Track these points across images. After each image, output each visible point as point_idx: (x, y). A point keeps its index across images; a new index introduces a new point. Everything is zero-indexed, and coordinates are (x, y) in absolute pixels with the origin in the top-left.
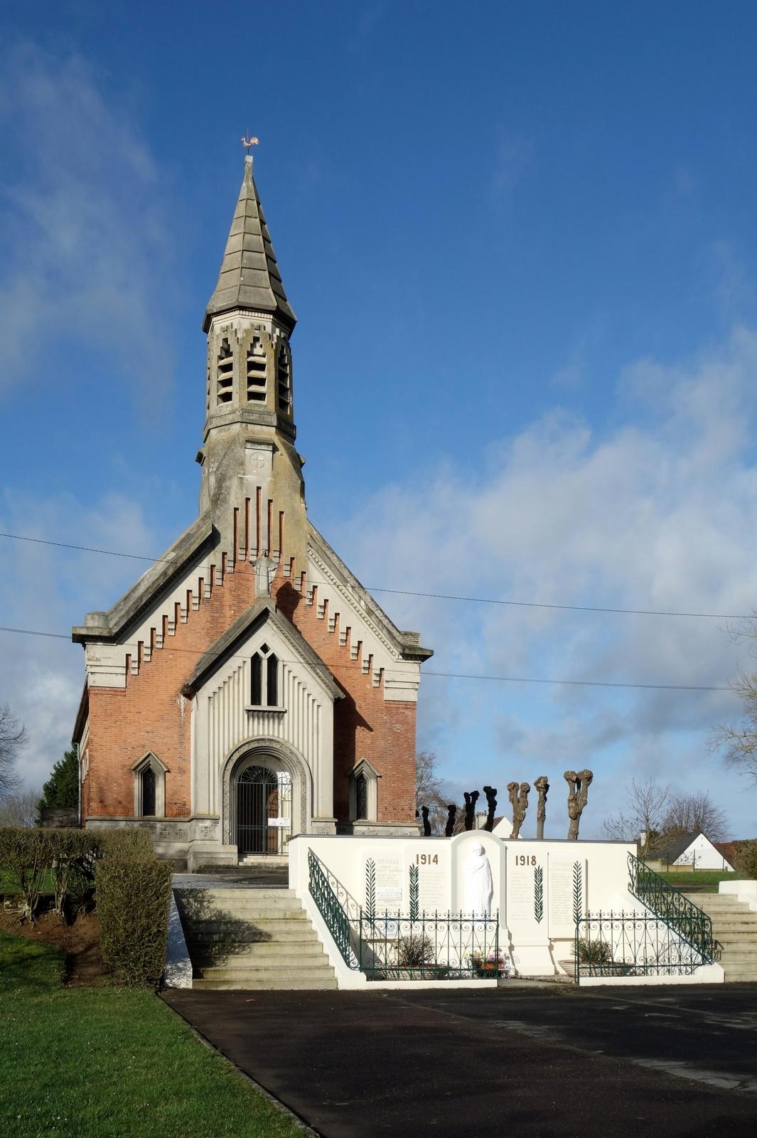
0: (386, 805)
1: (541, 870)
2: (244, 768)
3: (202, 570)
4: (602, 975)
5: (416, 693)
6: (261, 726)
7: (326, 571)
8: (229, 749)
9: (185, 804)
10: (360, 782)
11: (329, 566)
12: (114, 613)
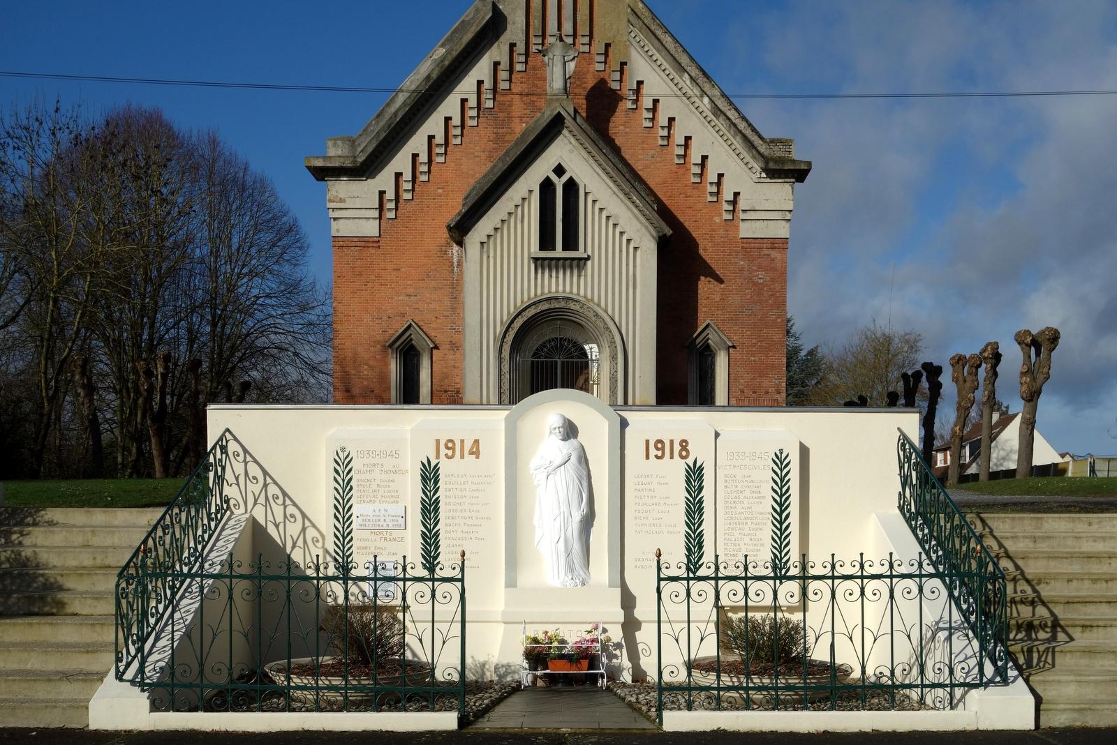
0: (741, 387)
1: (701, 468)
2: (534, 342)
3: (481, 70)
4: (689, 707)
5: (787, 225)
6: (554, 280)
7: (655, 58)
8: (509, 313)
9: (458, 392)
10: (706, 357)
11: (658, 50)
12: (363, 137)
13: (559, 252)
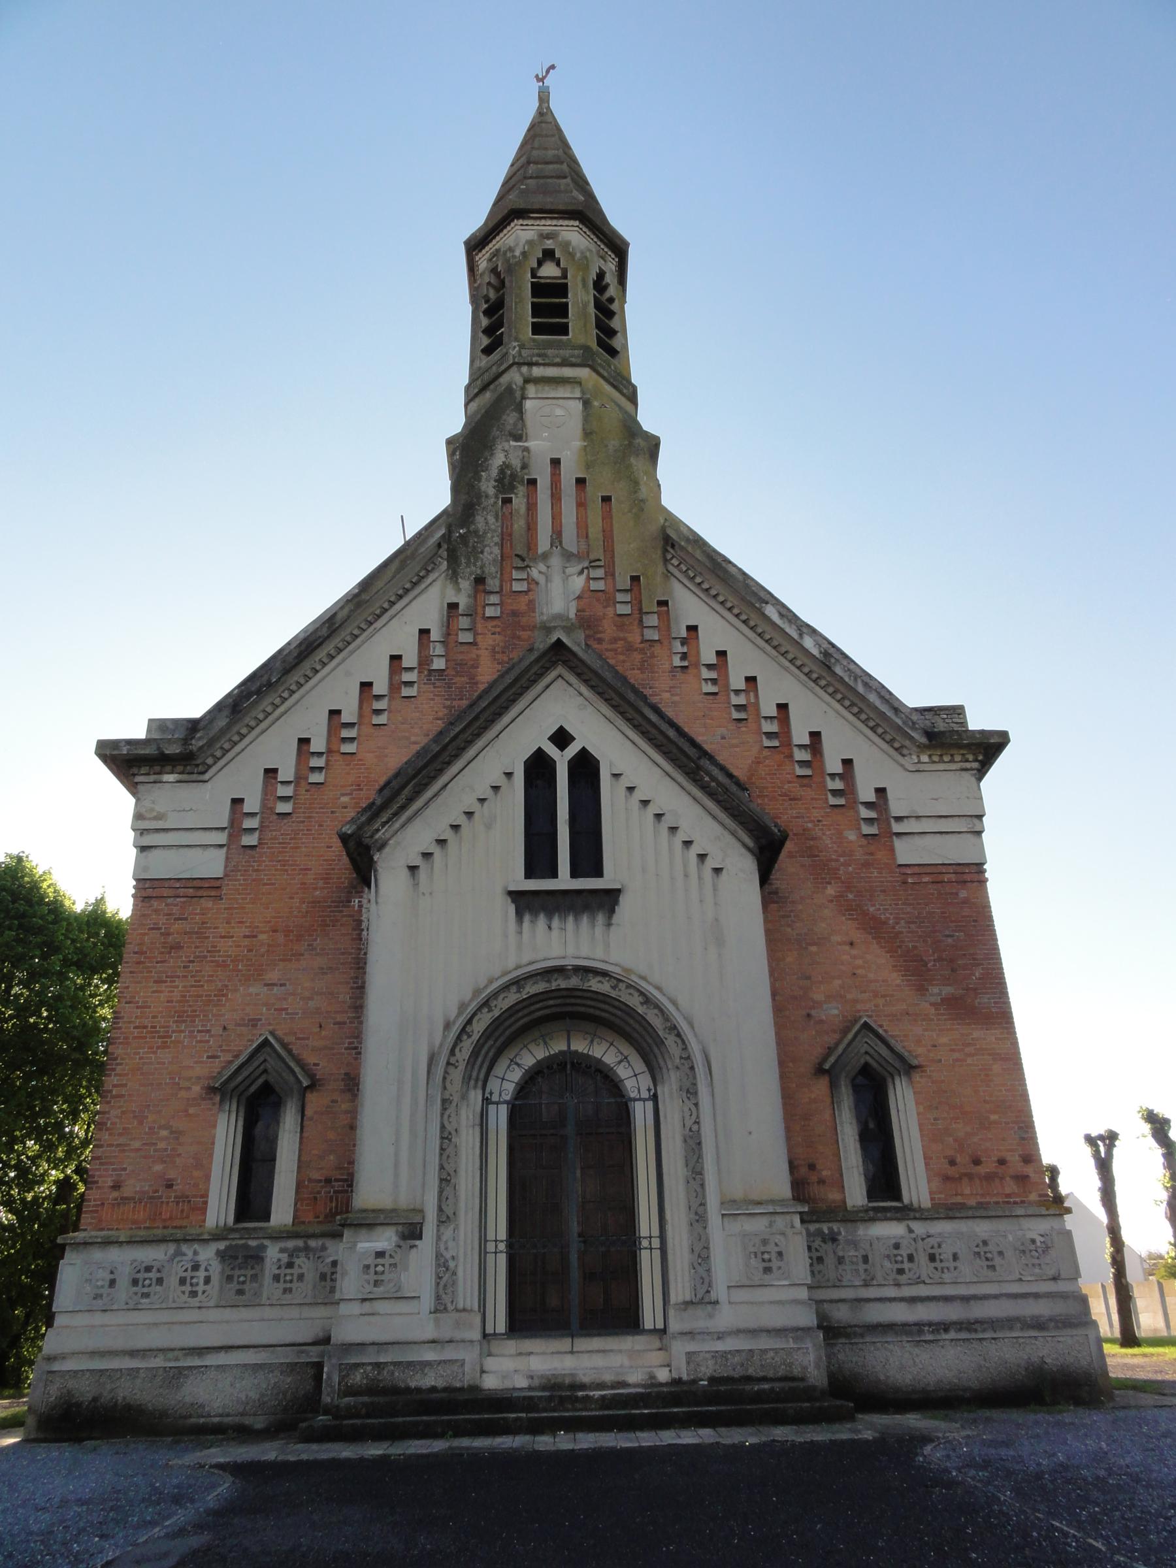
13: (564, 880)
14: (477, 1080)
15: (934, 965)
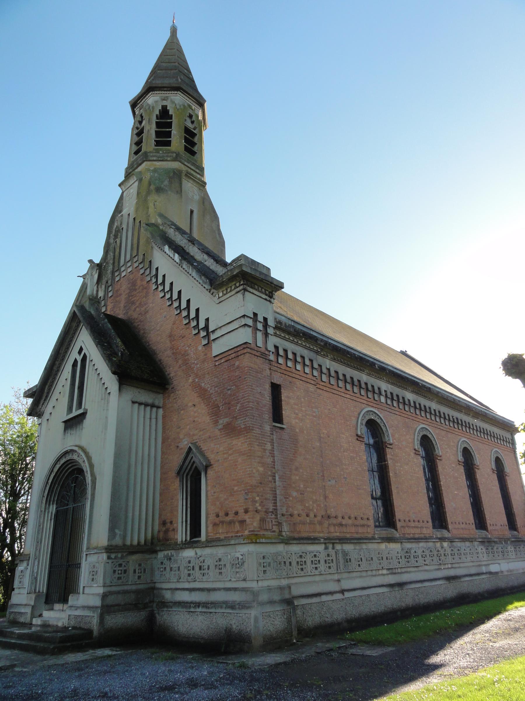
14: (53, 501)
15: (223, 408)
